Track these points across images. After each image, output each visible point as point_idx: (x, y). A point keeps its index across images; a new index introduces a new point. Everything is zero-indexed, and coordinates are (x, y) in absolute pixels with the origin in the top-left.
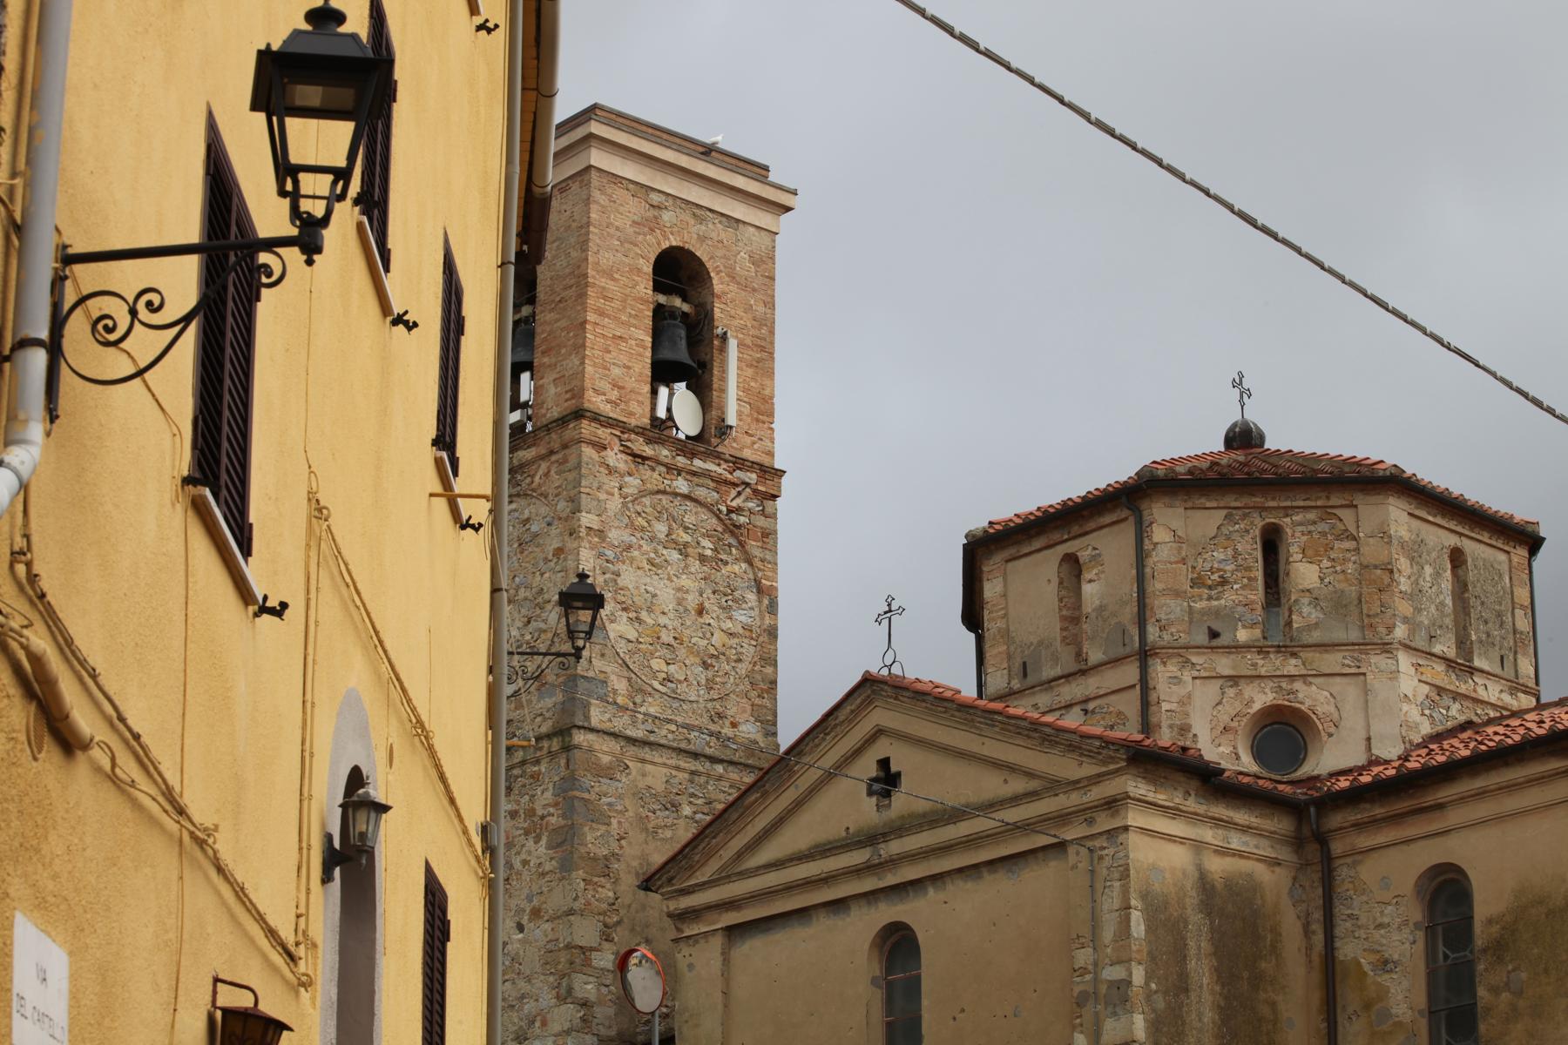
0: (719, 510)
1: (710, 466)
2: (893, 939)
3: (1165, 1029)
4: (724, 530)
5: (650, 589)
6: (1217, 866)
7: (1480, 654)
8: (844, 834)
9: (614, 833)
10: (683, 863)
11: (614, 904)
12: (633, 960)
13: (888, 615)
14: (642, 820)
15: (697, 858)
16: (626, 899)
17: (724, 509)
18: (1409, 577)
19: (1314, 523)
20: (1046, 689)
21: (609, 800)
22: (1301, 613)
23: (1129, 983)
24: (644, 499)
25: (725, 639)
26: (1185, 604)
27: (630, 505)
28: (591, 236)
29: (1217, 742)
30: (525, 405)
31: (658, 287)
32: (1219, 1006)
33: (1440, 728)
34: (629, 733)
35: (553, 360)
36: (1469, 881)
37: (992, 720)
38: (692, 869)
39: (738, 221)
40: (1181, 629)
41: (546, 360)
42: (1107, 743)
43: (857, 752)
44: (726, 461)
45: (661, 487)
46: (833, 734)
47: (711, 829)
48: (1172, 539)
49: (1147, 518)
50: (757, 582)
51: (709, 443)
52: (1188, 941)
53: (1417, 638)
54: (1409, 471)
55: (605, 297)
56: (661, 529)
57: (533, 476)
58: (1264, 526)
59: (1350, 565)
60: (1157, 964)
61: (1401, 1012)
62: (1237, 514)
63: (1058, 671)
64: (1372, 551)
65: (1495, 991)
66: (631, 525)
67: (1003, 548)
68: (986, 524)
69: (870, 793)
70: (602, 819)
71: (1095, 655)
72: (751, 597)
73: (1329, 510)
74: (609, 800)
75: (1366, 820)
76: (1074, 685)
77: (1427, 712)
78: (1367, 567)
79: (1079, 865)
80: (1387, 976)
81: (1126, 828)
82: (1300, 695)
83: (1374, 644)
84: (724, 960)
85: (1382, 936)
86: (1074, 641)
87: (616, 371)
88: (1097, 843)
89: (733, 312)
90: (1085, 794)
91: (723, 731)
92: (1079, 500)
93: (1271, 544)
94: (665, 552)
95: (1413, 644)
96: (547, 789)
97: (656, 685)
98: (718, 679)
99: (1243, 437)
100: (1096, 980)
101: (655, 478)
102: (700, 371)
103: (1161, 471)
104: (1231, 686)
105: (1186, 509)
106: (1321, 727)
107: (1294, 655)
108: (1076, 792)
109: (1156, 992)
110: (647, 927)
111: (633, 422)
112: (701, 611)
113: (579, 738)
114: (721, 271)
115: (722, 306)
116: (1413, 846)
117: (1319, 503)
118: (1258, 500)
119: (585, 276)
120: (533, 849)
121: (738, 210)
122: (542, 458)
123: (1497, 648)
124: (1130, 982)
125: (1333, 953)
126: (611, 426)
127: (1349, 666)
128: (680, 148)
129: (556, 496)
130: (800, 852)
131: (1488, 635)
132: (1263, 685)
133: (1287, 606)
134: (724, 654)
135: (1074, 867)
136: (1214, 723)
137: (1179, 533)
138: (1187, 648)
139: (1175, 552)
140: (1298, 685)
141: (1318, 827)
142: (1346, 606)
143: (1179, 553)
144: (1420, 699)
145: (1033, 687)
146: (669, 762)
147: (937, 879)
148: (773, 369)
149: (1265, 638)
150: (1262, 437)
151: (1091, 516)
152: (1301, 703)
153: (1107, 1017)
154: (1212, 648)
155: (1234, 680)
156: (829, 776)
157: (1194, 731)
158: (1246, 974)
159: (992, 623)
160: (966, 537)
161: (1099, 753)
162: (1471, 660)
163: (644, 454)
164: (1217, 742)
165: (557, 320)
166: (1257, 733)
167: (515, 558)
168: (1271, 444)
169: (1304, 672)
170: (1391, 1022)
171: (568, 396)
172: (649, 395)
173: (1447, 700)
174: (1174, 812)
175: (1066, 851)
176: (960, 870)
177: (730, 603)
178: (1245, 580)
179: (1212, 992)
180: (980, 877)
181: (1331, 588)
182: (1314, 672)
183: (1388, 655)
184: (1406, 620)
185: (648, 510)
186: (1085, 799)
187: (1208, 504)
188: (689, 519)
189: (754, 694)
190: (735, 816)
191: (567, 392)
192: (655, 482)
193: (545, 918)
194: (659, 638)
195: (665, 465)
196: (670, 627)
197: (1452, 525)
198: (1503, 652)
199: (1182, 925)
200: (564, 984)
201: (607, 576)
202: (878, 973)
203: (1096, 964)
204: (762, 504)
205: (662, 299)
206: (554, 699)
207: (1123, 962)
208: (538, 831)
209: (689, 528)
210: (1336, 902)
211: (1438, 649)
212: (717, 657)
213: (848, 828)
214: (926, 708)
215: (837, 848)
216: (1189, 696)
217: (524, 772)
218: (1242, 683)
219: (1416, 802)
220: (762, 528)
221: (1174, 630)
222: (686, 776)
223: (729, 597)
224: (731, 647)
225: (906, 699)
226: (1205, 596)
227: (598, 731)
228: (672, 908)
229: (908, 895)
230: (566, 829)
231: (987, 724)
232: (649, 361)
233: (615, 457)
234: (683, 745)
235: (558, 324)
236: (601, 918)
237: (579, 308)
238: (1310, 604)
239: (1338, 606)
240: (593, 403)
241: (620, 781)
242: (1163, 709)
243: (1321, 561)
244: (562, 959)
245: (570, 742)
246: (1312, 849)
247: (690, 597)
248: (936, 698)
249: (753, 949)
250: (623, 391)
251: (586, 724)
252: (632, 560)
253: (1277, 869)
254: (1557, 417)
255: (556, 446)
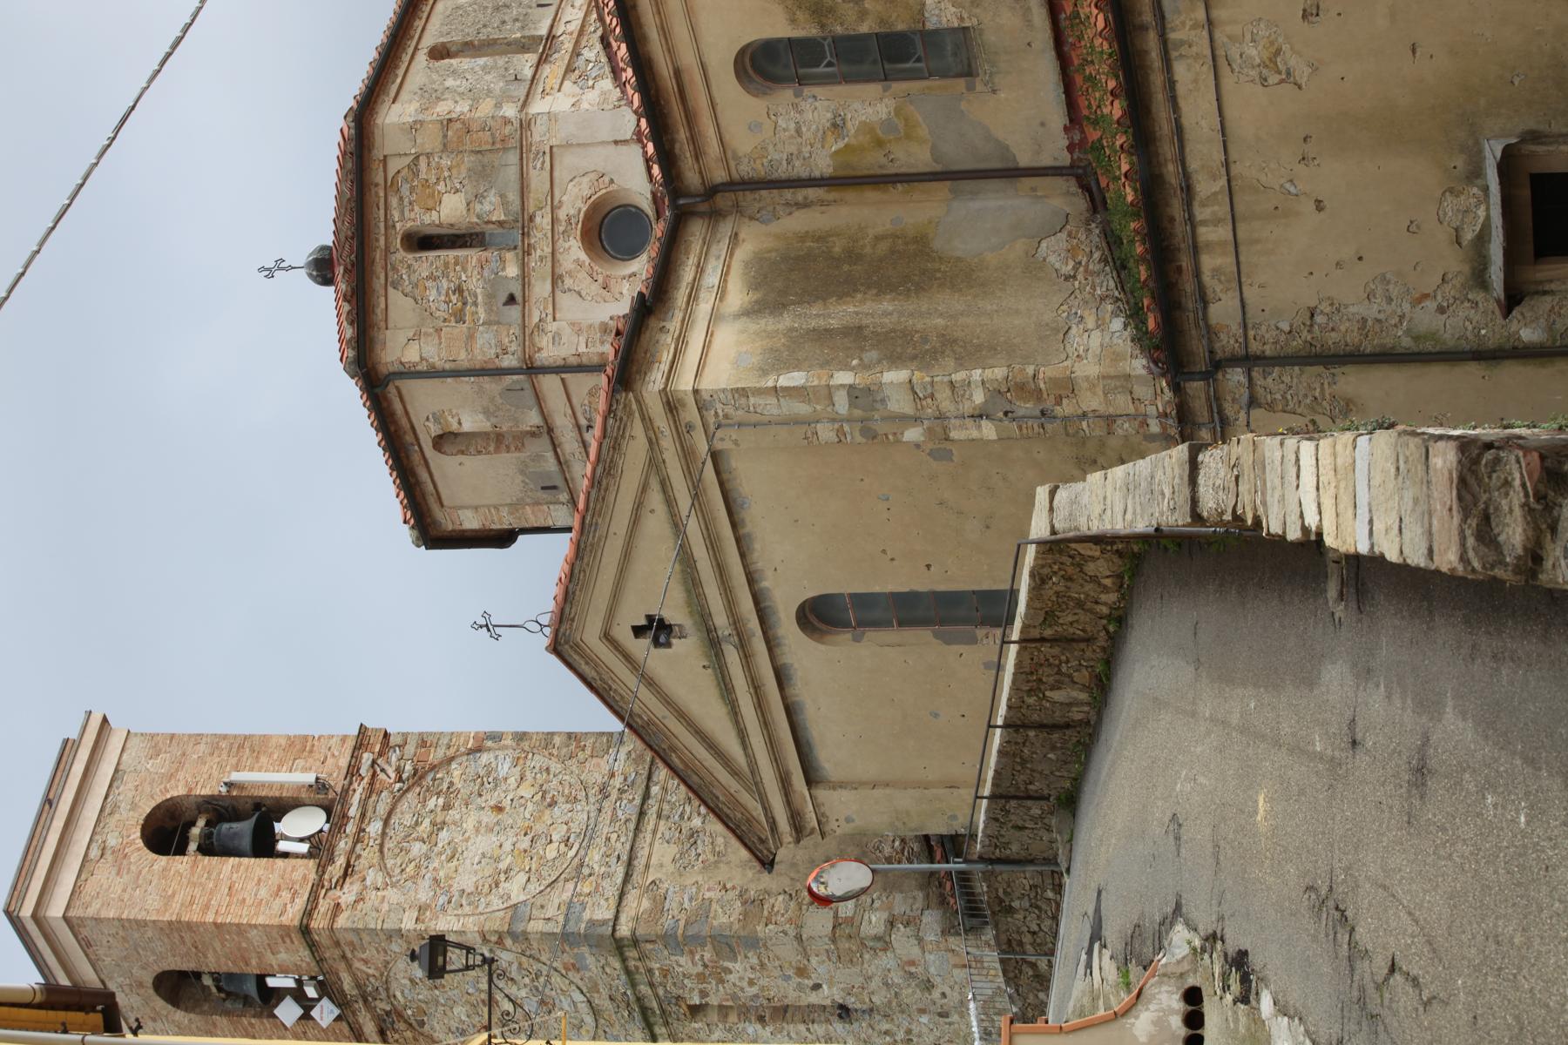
0: (398, 791)
1: (355, 800)
2: (813, 619)
3: (899, 350)
4: (419, 785)
5: (477, 860)
6: (737, 297)
7: (535, 28)
8: (710, 671)
9: (719, 895)
10: (744, 828)
11: (791, 895)
12: (820, 890)
13: (491, 627)
14: (706, 867)
15: (739, 816)
16: (785, 882)
17: (398, 785)
18: (456, 102)
19: (401, 198)
20: (568, 467)
21: (686, 900)
22: (490, 212)
23: (851, 387)
24: (388, 866)
25: (526, 784)
26: (481, 328)
27: (394, 880)
28: (132, 917)
29: (618, 296)
30: (299, 982)
31: (181, 850)
32: (877, 295)
33: (607, 69)
34: (619, 881)
35: (254, 955)
36: (748, 45)
37: (591, 525)
38: (750, 820)
39: (116, 770)
40: (505, 333)
41: (254, 962)
42: (610, 411)
43: (627, 657)
44: (351, 783)
45: (377, 848)
46: (610, 682)
47: (709, 801)
48: (416, 342)
49: (396, 368)
50: (471, 752)
51: (333, 801)
52: (811, 327)
53: (515, 94)
54: (352, 103)
55: (191, 903)
56: (417, 849)
57: (368, 975)
58: (405, 250)
59: (443, 162)
60: (833, 359)
61: (885, 110)
62: (392, 276)
63: (550, 455)
64: (429, 140)
65: (863, 14)
66: (414, 878)
67: (429, 510)
68: (406, 527)
69: (668, 645)
70: (704, 910)
71: (533, 419)
72: (485, 758)
73: (389, 183)
74: (686, 900)
75: (692, 148)
76: (563, 440)
77: (590, 83)
78: (445, 145)
79: (734, 438)
80: (849, 124)
81: (696, 392)
82: (572, 212)
83: (521, 139)
84: (841, 787)
85: (808, 130)
86: (522, 439)
87: (263, 893)
88: (711, 420)
89: (205, 776)
90: (662, 432)
91: (618, 786)
92: (380, 435)
93: (423, 242)
94: (440, 845)
95: (522, 99)
96: (677, 962)
97: (572, 853)
98: (566, 791)
99: (322, 269)
100: (849, 420)
101: (368, 855)
102: (263, 809)
103: (350, 353)
104: (563, 282)
105: (387, 329)
106: (604, 191)
107: (531, 219)
108: (660, 442)
109: (861, 359)
110: (813, 861)
111: (313, 876)
112: (499, 809)
113: (624, 930)
114: (165, 788)
115: (199, 787)
116: (718, 100)
117: (382, 194)
118: (378, 256)
119: (170, 923)
120: (738, 975)
121: (106, 770)
122: (349, 966)
123: (530, 11)
124: (851, 386)
125: (827, 179)
126: (316, 898)
127: (543, 162)
128: (46, 827)
129: (386, 952)
130: (729, 713)
131: (517, 20)
132: (561, 250)
133: (484, 226)
134: (542, 786)
135: (736, 443)
136: (599, 299)
137: (411, 335)
138: (524, 327)
139: (430, 339)
140: (562, 214)
141: (697, 196)
142: (483, 166)
143: (430, 335)
144: (576, 89)
145: (566, 480)
146: (648, 840)
147: (751, 579)
148: (261, 736)
149: (515, 248)
150: (323, 248)
151: (395, 422)
152: (580, 211)
153: (886, 408)
154: (524, 302)
155: (556, 279)
156: (650, 683)
157: (607, 319)
158: (846, 268)
159: (504, 521)
160: (418, 546)
161: (621, 419)
162: (541, 38)
163: (344, 865)
164: (618, 296)
165: (215, 950)
166: (609, 254)
167: (449, 993)
168: (328, 239)
169: (549, 208)
170: (895, 120)
171: (288, 941)
172: (286, 860)
173: (580, 62)
174: (681, 342)
175: (720, 451)
176: (743, 556)
177: (490, 780)
178: (458, 268)
179: (863, 302)
180: (749, 535)
181: (465, 182)
182: (549, 198)
183: (533, 124)
184: (498, 106)
185: (399, 861)
186: (667, 432)
187: (383, 306)
188: (408, 820)
189: (581, 756)
190: (695, 778)
191: (284, 942)
192: (371, 854)
193: (806, 963)
194: (525, 851)
195: (355, 844)
196: (515, 839)
197: (406, 58)
198: (534, 5)
199: (794, 334)
200: (872, 944)
201: (464, 903)
202: (849, 636)
203: (833, 420)
204: (394, 747)
205: (193, 846)
206: (587, 955)
207: (830, 393)
208: (719, 971)
209: (417, 820)
210: (775, 176)
211: (528, 73)
212: (545, 792)
213: (704, 667)
214: (581, 591)
215: (723, 677)
216: (573, 324)
217: (660, 984)
218: (559, 271)
219: (673, 99)
220: (417, 748)
221: (507, 340)
222: (662, 822)
223: (485, 781)
224: (535, 778)
225: (573, 611)
226: (473, 308)
227: (618, 912)
228: (791, 839)
229: (769, 607)
230: (716, 943)
231: (595, 530)
232: (253, 860)
233: (347, 895)
234: (632, 826)
235: (218, 949)
236: (804, 907)
237: (201, 929)
238: (481, 203)
239: (483, 174)
240: (294, 916)
241: (668, 889)
242: (585, 350)
243: (439, 192)
244: (847, 945)
245: (628, 940)
246: (723, 201)
247: (485, 820)
248: (570, 581)
249: (829, 758)
250: (283, 887)
251: (611, 924)
252: (448, 878)
253: (742, 236)
254: (193, 21)
255: (337, 952)
